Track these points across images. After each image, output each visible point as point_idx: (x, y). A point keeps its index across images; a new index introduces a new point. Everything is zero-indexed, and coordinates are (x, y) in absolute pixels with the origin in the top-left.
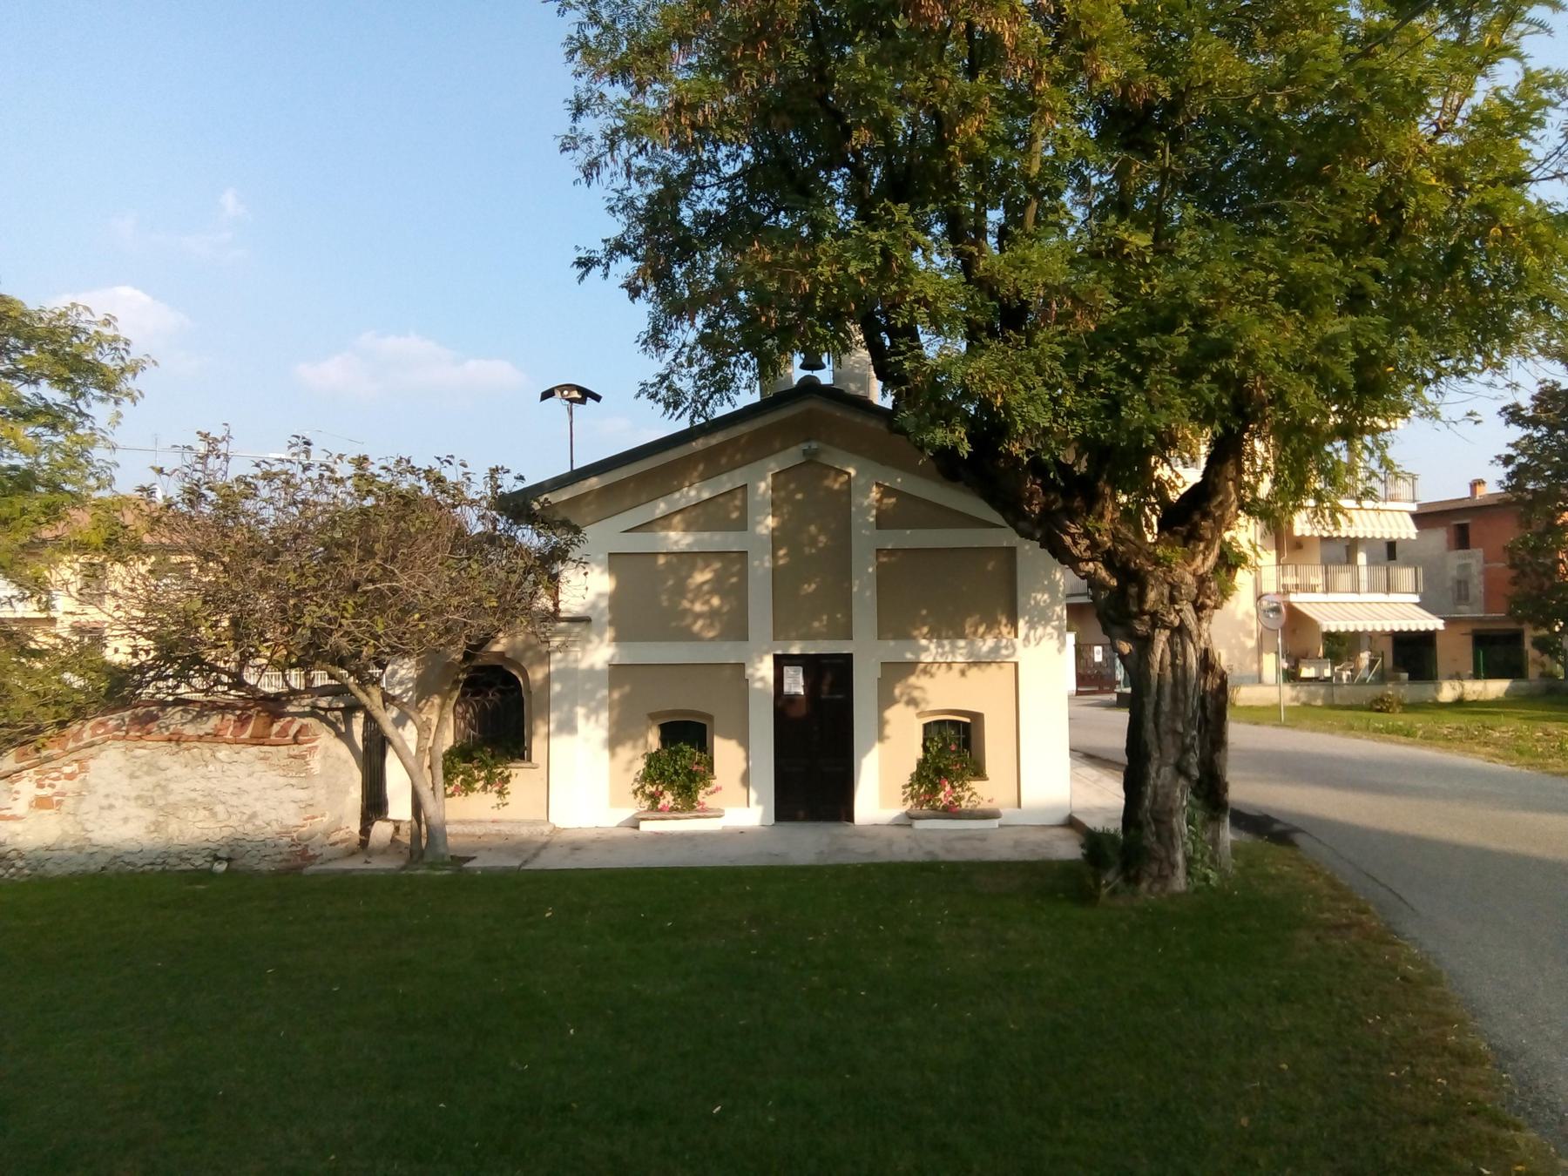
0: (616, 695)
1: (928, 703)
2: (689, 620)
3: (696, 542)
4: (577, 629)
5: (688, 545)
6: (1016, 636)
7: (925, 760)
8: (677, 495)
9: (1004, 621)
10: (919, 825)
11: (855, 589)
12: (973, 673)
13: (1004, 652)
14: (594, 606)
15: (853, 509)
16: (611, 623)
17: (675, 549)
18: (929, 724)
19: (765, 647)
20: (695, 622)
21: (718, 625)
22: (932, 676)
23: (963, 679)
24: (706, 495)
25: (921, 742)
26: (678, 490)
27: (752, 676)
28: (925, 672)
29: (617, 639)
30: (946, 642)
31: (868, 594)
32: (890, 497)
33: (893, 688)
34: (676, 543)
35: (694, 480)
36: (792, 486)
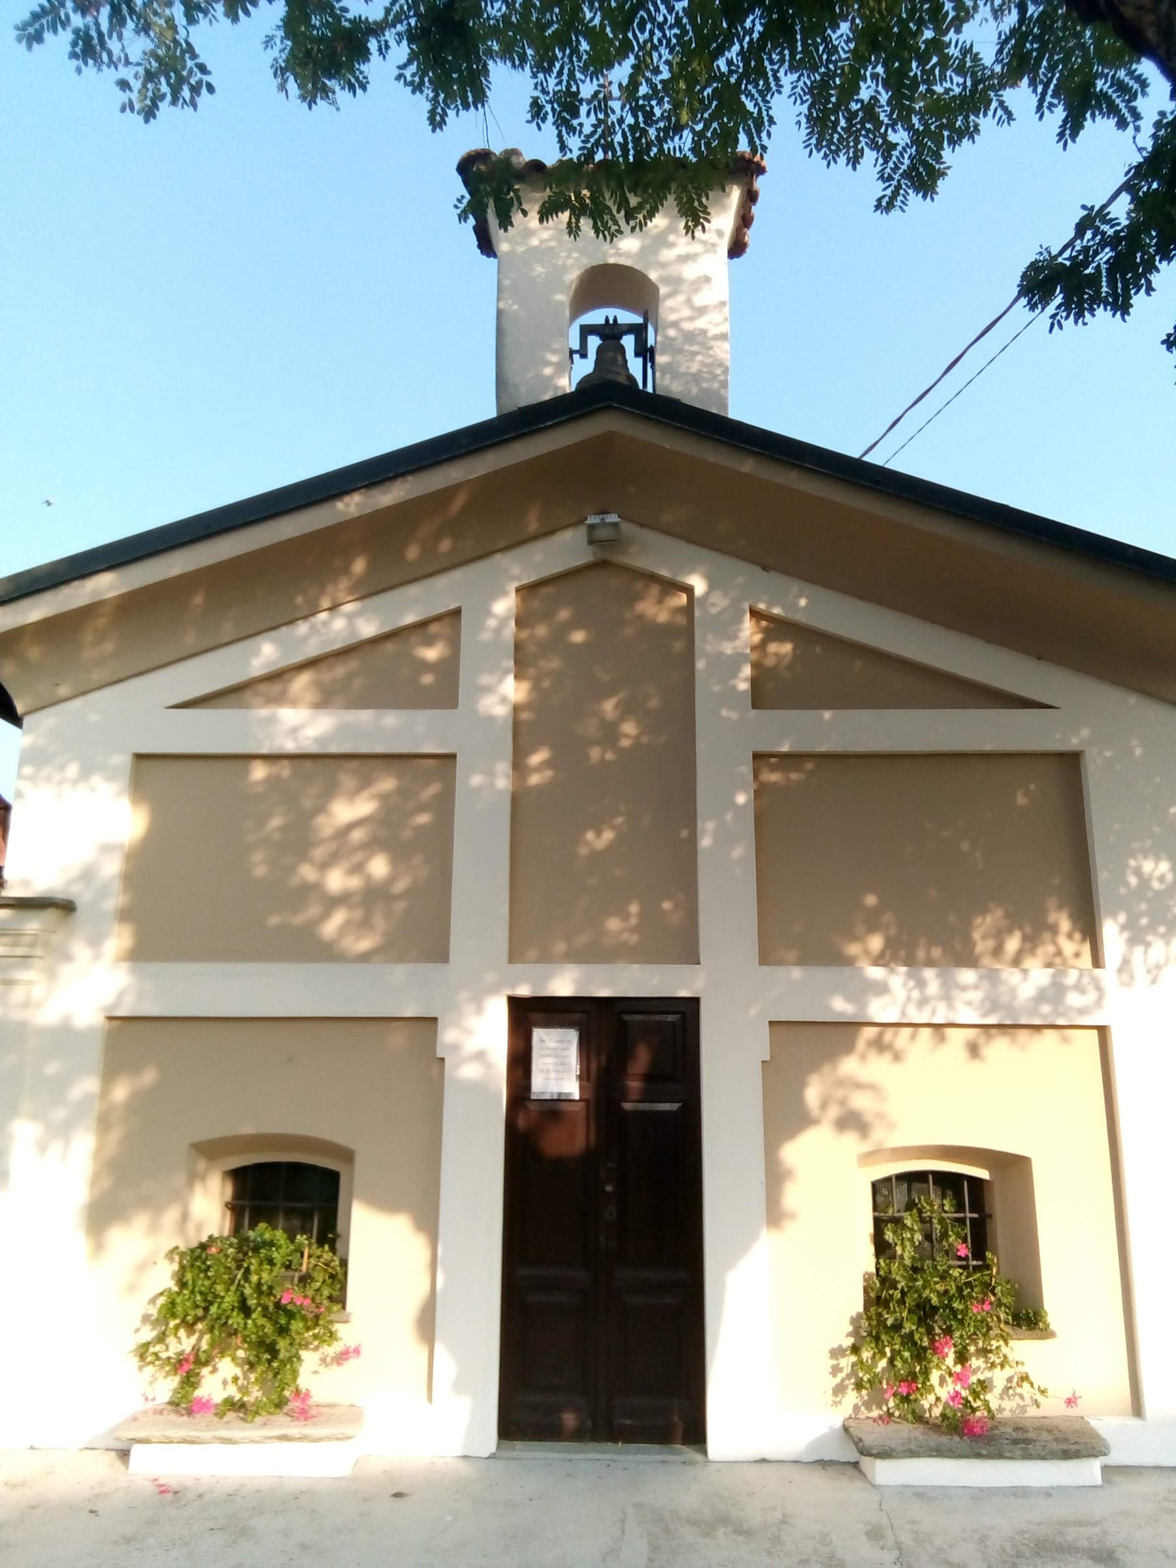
0: (121, 1092)
1: (891, 1126)
2: (313, 911)
3: (340, 731)
4: (33, 924)
5: (318, 740)
6: (1097, 961)
7: (886, 1281)
8: (302, 628)
9: (1065, 925)
10: (886, 1472)
11: (705, 842)
12: (999, 1049)
13: (1073, 999)
14: (87, 875)
15: (700, 665)
16: (124, 915)
17: (290, 746)
18: (887, 1180)
19: (490, 978)
20: (326, 915)
21: (379, 921)
22: (897, 1057)
23: (976, 1064)
24: (368, 629)
25: (870, 1229)
26: (305, 618)
27: (456, 1048)
28: (879, 1045)
29: (138, 955)
30: (929, 974)
31: (737, 852)
32: (781, 640)
33: (801, 1085)
34: (294, 731)
35: (342, 596)
36: (564, 614)
